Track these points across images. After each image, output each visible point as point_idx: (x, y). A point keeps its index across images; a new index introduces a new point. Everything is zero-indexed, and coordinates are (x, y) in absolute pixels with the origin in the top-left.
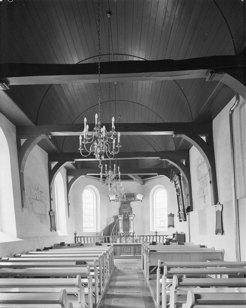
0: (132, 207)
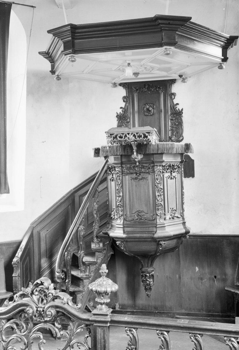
0: (179, 107)
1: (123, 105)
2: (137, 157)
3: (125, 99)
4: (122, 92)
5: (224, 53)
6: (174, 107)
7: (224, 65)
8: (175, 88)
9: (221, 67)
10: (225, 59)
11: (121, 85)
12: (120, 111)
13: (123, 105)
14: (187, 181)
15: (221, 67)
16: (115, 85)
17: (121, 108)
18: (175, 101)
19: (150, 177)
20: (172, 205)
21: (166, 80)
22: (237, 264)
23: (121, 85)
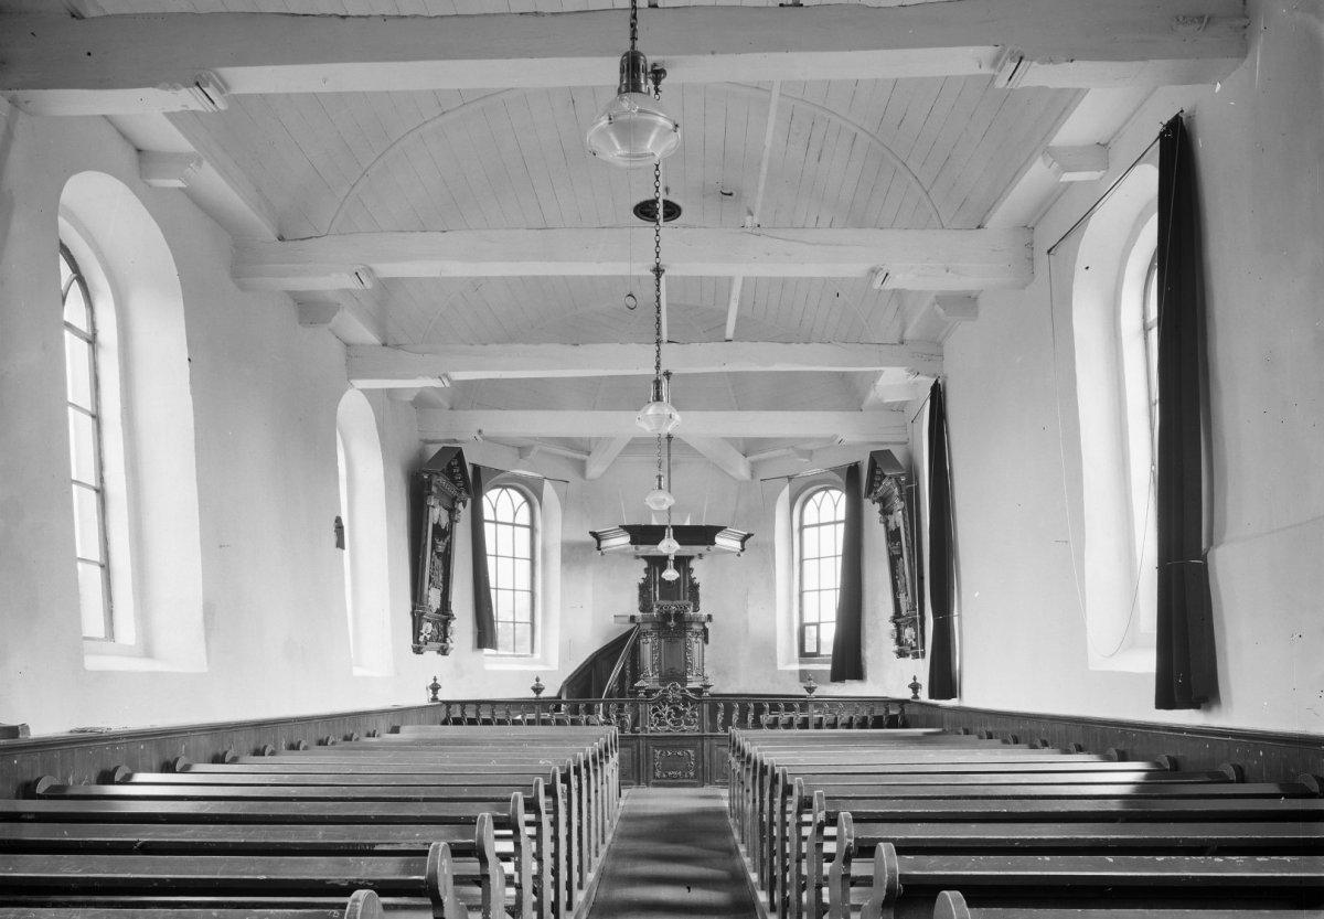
0: (696, 581)
1: (645, 576)
2: (672, 623)
3: (647, 570)
4: (645, 564)
5: (743, 546)
6: (691, 580)
7: (742, 554)
8: (693, 564)
9: (739, 555)
10: (743, 550)
11: (644, 557)
12: (642, 581)
13: (645, 576)
14: (706, 647)
15: (739, 555)
16: (637, 557)
17: (709, 618)
18: (693, 576)
19: (682, 641)
20: (697, 665)
21: (481, 380)
22: (400, 874)
23: (644, 557)
